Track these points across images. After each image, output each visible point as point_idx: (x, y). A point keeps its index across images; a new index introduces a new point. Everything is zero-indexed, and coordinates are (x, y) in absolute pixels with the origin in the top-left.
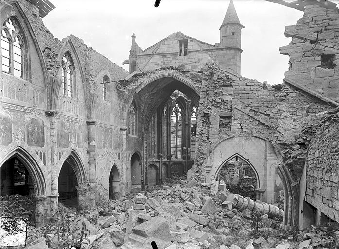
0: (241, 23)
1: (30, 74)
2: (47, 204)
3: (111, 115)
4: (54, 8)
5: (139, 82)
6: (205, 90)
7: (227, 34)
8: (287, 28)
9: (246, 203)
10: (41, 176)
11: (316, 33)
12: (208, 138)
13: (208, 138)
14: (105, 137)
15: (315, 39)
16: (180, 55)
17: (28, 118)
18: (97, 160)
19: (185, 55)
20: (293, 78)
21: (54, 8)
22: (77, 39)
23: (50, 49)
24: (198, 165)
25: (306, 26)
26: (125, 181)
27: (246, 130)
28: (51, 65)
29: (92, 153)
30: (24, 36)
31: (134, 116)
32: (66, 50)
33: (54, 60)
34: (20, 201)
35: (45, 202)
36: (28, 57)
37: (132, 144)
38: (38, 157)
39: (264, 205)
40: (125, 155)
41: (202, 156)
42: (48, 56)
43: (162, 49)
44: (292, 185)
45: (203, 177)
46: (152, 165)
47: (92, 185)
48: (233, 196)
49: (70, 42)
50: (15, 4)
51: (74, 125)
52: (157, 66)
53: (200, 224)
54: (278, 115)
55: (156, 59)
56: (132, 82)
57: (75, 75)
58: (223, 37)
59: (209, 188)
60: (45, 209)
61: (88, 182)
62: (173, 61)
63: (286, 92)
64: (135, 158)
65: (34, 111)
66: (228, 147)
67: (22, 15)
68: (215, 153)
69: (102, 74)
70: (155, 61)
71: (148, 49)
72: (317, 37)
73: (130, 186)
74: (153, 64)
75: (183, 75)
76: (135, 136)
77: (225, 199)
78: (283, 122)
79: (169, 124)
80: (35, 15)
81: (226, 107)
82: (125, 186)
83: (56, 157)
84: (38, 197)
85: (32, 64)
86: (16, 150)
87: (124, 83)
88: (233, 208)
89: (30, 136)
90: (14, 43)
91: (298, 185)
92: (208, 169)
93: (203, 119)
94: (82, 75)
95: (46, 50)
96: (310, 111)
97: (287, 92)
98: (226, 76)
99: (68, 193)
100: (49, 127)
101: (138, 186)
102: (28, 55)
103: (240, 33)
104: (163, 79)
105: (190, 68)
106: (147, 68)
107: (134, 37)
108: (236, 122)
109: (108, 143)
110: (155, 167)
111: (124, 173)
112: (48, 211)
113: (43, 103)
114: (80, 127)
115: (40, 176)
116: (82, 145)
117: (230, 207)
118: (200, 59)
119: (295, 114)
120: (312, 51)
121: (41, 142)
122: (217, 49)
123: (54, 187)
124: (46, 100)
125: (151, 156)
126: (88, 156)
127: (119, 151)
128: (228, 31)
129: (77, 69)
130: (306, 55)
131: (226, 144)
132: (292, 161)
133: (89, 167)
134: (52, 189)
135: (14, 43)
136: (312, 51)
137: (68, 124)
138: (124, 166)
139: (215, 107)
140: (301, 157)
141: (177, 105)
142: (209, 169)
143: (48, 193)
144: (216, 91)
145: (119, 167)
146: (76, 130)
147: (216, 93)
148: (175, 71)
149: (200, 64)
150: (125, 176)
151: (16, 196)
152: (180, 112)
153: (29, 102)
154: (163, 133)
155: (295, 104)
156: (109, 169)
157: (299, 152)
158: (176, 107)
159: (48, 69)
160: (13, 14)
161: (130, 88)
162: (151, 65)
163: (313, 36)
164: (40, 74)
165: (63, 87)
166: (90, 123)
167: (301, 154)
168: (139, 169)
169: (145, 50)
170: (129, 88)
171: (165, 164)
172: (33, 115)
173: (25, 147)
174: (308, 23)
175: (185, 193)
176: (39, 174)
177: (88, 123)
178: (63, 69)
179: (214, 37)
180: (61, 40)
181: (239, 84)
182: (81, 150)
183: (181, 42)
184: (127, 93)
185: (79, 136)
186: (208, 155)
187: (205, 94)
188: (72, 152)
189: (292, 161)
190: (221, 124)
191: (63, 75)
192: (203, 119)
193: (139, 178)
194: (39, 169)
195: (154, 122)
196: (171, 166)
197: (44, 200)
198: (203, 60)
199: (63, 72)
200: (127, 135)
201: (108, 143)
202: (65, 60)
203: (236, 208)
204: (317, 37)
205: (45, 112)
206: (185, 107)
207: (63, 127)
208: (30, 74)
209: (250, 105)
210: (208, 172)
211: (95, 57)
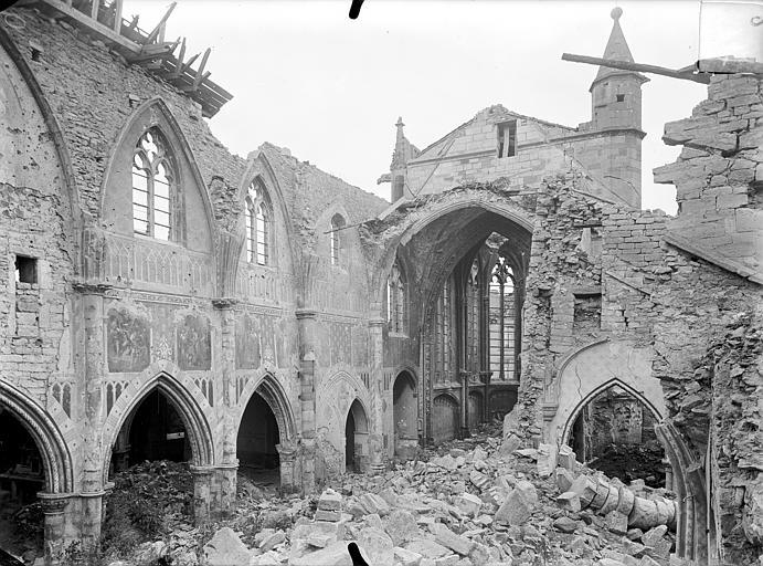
0: (644, 129)
1: (184, 230)
2: (216, 481)
3: (350, 295)
4: (231, 97)
5: (407, 223)
6: (542, 237)
7: (605, 101)
8: (668, 127)
9: (614, 499)
10: (205, 428)
11: (735, 134)
12: (548, 345)
13: (548, 345)
14: (335, 343)
15: (733, 147)
16: (501, 156)
17: (179, 316)
18: (318, 392)
19: (511, 153)
20: (684, 233)
21: (231, 97)
22: (279, 150)
23: (222, 179)
24: (526, 404)
25: (712, 121)
26: (379, 432)
27: (637, 325)
28: (224, 211)
29: (307, 378)
30: (174, 160)
31: (402, 293)
32: (255, 174)
33: (228, 199)
34: (170, 473)
35: (213, 479)
36: (181, 199)
37: (396, 351)
38: (199, 390)
39: (659, 503)
40: (380, 377)
41: (535, 385)
42: (217, 194)
43: (461, 146)
44: (691, 469)
45: (538, 431)
46: (444, 396)
47: (309, 443)
48: (584, 482)
49: (262, 157)
50: (157, 104)
51: (270, 322)
52: (448, 183)
53: (455, 553)
54: (652, 314)
55: (446, 168)
56: (392, 223)
57: (273, 222)
58: (598, 108)
59: (535, 461)
60: (211, 493)
61: (300, 436)
62: (485, 170)
63: (670, 264)
64: (404, 381)
65: (190, 301)
66: (595, 364)
67: (169, 123)
68: (565, 377)
69: (330, 212)
70: (444, 172)
71: (430, 147)
72: (738, 142)
73: (391, 442)
74: (442, 179)
75: (505, 200)
76: (404, 336)
77: (568, 486)
78: (666, 330)
79: (484, 304)
80: (195, 118)
81: (590, 275)
82: (379, 444)
83: (232, 390)
84: (200, 468)
85: (187, 211)
86: (158, 379)
87: (376, 226)
88: (584, 509)
89: (183, 351)
90: (156, 177)
91: (703, 470)
92: (547, 413)
93: (538, 302)
94: (287, 220)
95: (215, 181)
96: (726, 305)
97: (673, 264)
98: (589, 205)
99: (268, 455)
100: (220, 330)
101: (411, 442)
102: (180, 195)
103: (639, 95)
104: (459, 212)
105: (521, 182)
106: (430, 189)
107: (400, 125)
108: (612, 307)
109: (341, 353)
110: (452, 400)
111: (378, 415)
112: (219, 497)
113: (208, 284)
114: (282, 326)
115: (202, 427)
116: (286, 361)
117: (576, 506)
118: (543, 162)
119: (691, 313)
120: (725, 173)
121: (203, 361)
122: (583, 136)
123: (228, 448)
124: (214, 279)
125: (439, 375)
126: (299, 384)
127: (364, 370)
128: (608, 94)
129: (277, 209)
130: (712, 184)
131: (589, 358)
132: (683, 419)
133: (302, 405)
134: (225, 454)
135: (156, 177)
136: (725, 173)
137: (258, 320)
138: (378, 401)
139: (564, 274)
140: (700, 411)
141: (502, 260)
142: (550, 413)
143: (217, 460)
144: (566, 240)
145: (366, 404)
146: (274, 332)
147: (567, 244)
148: (486, 193)
149: (543, 171)
150: (379, 421)
151: (163, 464)
152: (510, 275)
153: (181, 284)
154: (469, 324)
155: (691, 291)
156: (345, 409)
157: (697, 398)
158: (499, 265)
159: (217, 218)
160: (154, 122)
161: (388, 237)
162: (435, 181)
163: (729, 142)
164: (204, 230)
165: (249, 248)
166: (303, 315)
167: (700, 403)
168: (414, 404)
169: (424, 151)
170: (385, 235)
171: (474, 392)
172: (190, 308)
173: (175, 372)
174: (716, 113)
175: (480, 470)
176: (201, 423)
177: (300, 316)
178: (248, 213)
179: (576, 110)
180: (245, 158)
181: (619, 222)
182: (285, 371)
183: (501, 127)
184: (382, 247)
185: (280, 343)
186: (548, 382)
187: (543, 245)
188: (267, 378)
189: (683, 419)
190: (578, 313)
191: (249, 224)
192: (538, 302)
193: (412, 424)
194: (200, 415)
195: (449, 301)
196: (492, 394)
197: (210, 474)
198: (555, 161)
199: (249, 218)
200: (385, 334)
201: (341, 353)
202: (253, 193)
203: (592, 508)
204: (738, 142)
205: (213, 302)
206: (521, 263)
207: (247, 327)
208: (184, 230)
209: (645, 269)
210: (549, 419)
211: (315, 179)
